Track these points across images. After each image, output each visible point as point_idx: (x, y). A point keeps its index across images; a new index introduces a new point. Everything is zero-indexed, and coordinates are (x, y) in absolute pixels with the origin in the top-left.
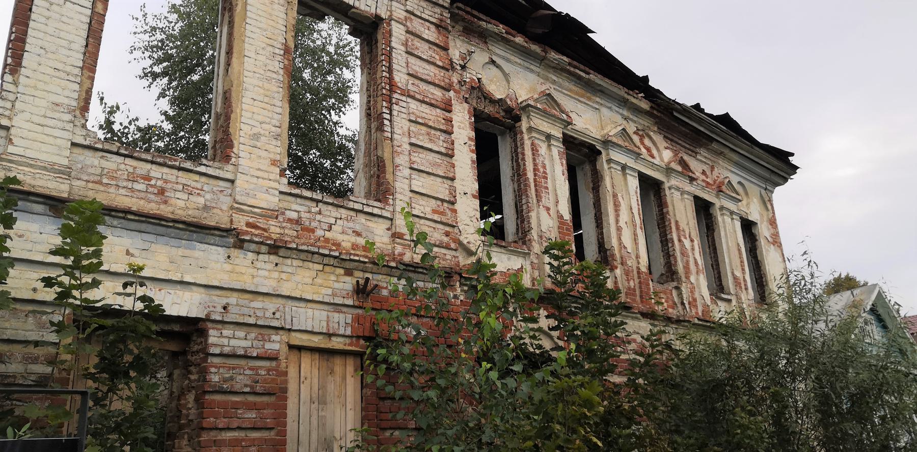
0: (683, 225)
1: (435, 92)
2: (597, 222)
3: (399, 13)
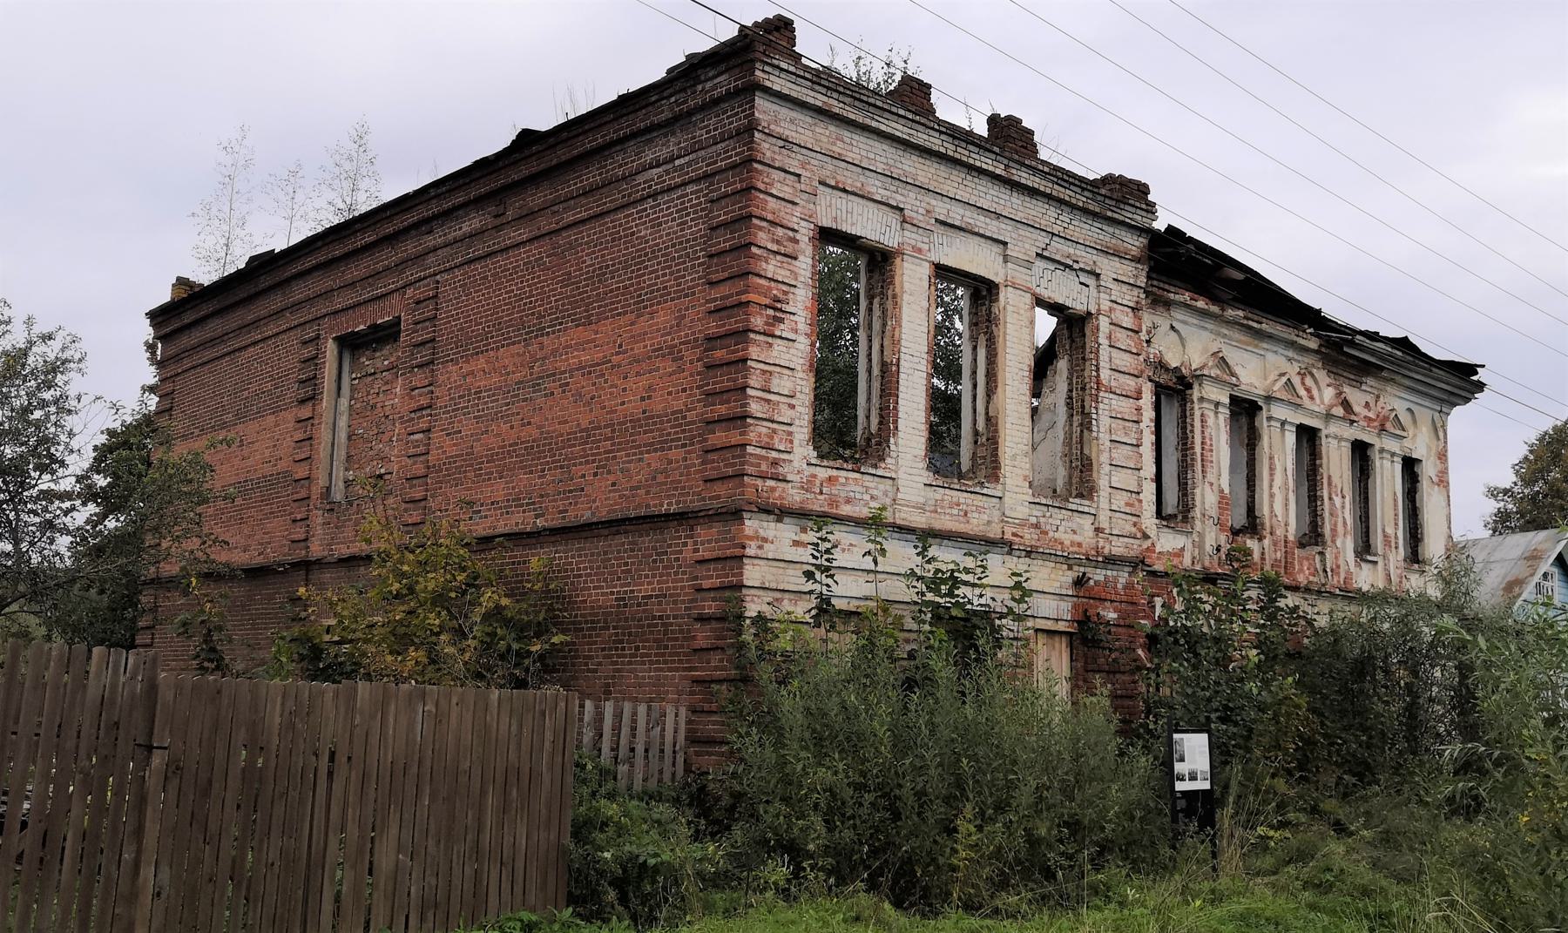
0: (1335, 480)
1: (1128, 382)
2: (1248, 482)
3: (1106, 305)
